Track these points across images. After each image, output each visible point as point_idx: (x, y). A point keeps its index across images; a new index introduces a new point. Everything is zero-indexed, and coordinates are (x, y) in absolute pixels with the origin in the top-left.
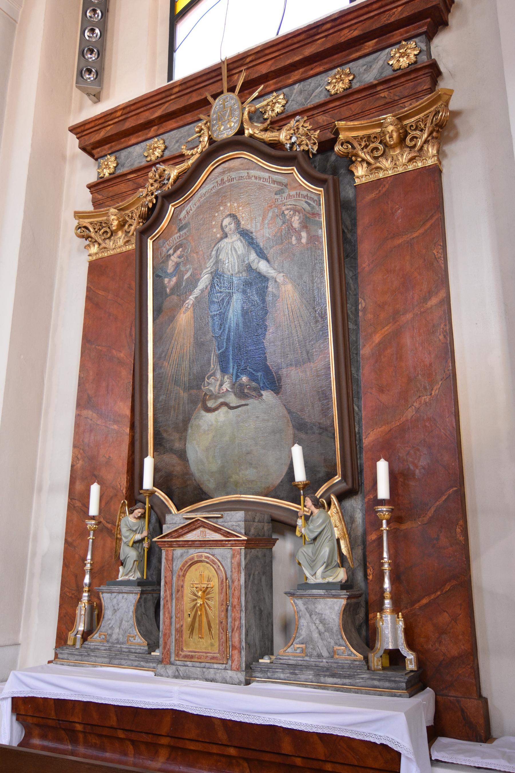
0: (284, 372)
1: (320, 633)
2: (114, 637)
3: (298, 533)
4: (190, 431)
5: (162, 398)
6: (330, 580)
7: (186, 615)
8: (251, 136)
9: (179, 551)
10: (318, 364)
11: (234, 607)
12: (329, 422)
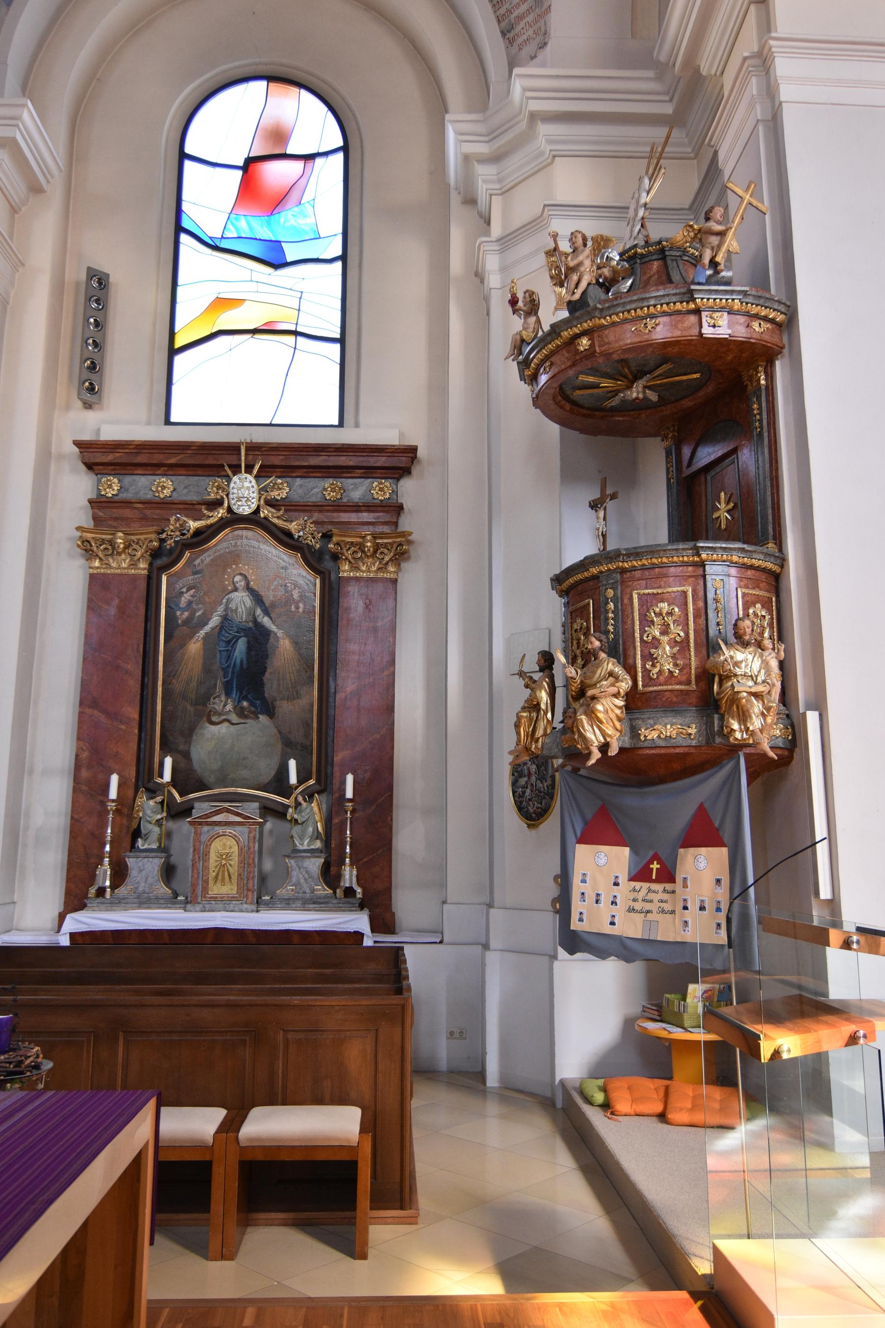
0: (278, 703)
1: (305, 880)
2: (141, 889)
3: (289, 818)
4: (194, 737)
5: (170, 708)
6: (312, 847)
7: (211, 871)
8: (265, 518)
9: (206, 828)
10: (303, 702)
11: (249, 865)
12: (309, 743)
